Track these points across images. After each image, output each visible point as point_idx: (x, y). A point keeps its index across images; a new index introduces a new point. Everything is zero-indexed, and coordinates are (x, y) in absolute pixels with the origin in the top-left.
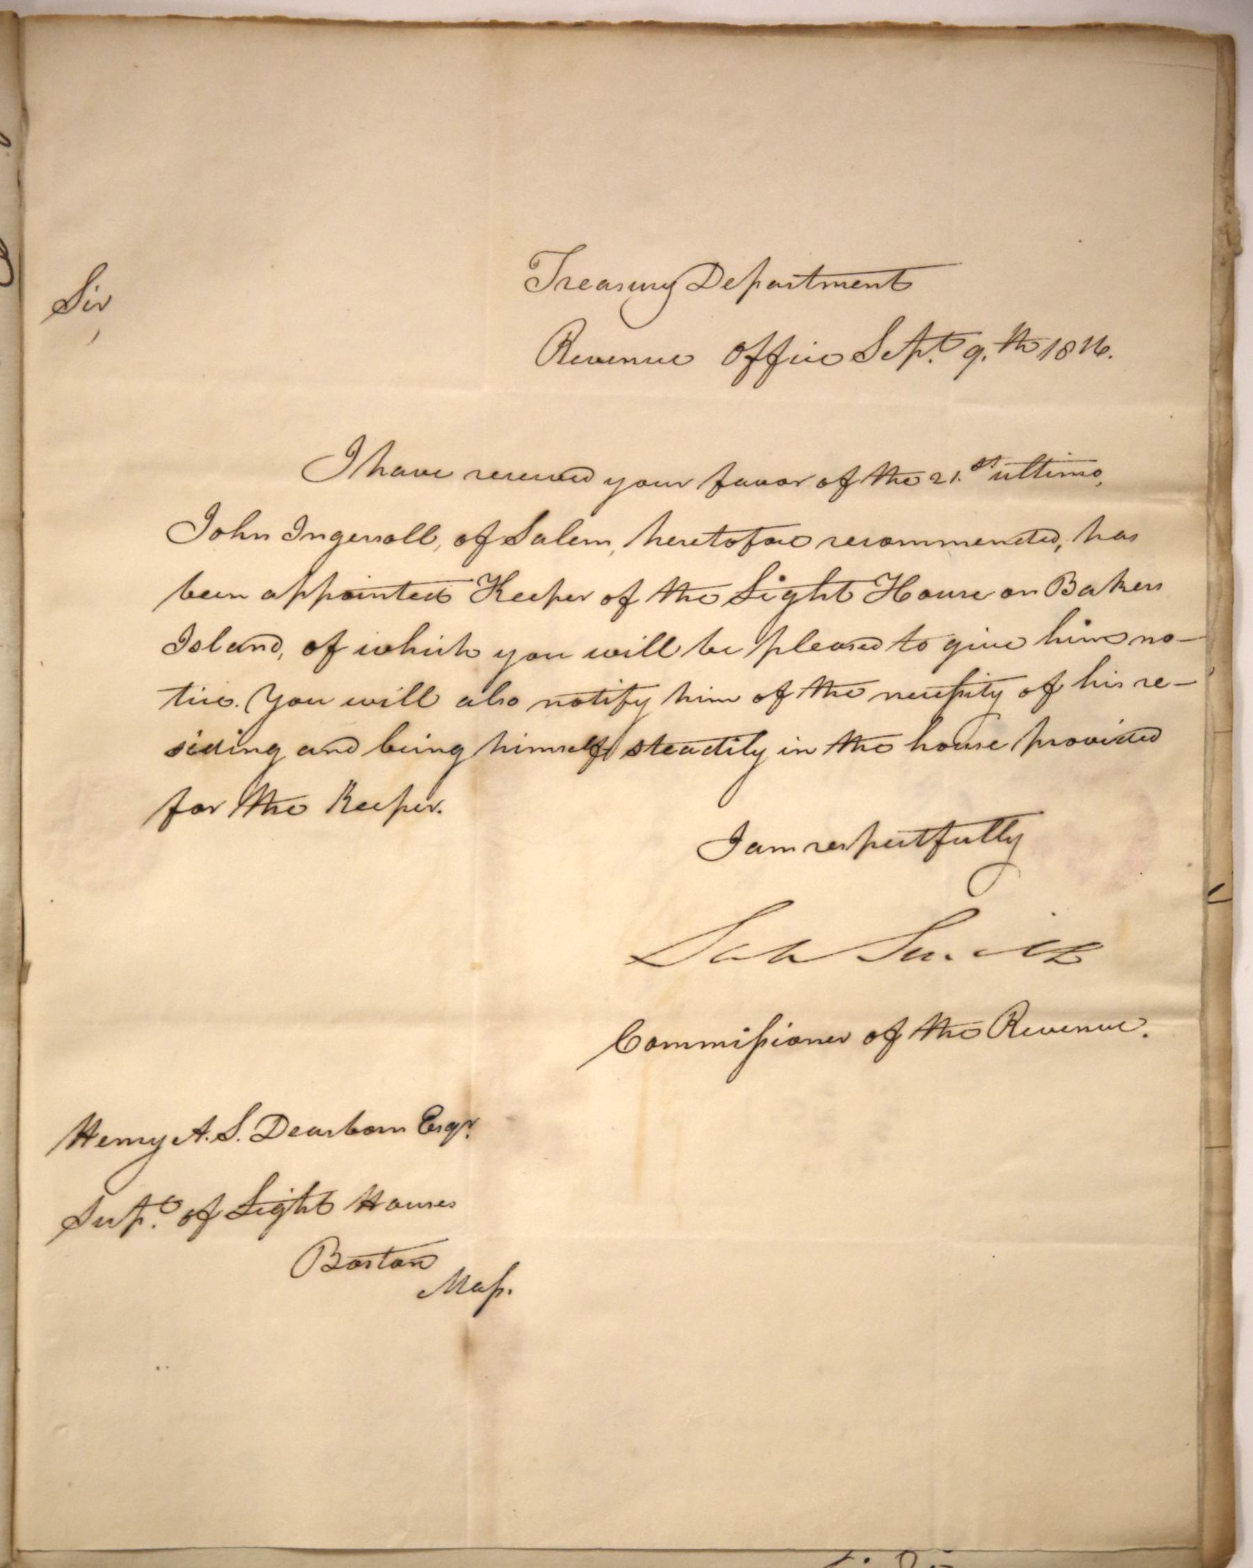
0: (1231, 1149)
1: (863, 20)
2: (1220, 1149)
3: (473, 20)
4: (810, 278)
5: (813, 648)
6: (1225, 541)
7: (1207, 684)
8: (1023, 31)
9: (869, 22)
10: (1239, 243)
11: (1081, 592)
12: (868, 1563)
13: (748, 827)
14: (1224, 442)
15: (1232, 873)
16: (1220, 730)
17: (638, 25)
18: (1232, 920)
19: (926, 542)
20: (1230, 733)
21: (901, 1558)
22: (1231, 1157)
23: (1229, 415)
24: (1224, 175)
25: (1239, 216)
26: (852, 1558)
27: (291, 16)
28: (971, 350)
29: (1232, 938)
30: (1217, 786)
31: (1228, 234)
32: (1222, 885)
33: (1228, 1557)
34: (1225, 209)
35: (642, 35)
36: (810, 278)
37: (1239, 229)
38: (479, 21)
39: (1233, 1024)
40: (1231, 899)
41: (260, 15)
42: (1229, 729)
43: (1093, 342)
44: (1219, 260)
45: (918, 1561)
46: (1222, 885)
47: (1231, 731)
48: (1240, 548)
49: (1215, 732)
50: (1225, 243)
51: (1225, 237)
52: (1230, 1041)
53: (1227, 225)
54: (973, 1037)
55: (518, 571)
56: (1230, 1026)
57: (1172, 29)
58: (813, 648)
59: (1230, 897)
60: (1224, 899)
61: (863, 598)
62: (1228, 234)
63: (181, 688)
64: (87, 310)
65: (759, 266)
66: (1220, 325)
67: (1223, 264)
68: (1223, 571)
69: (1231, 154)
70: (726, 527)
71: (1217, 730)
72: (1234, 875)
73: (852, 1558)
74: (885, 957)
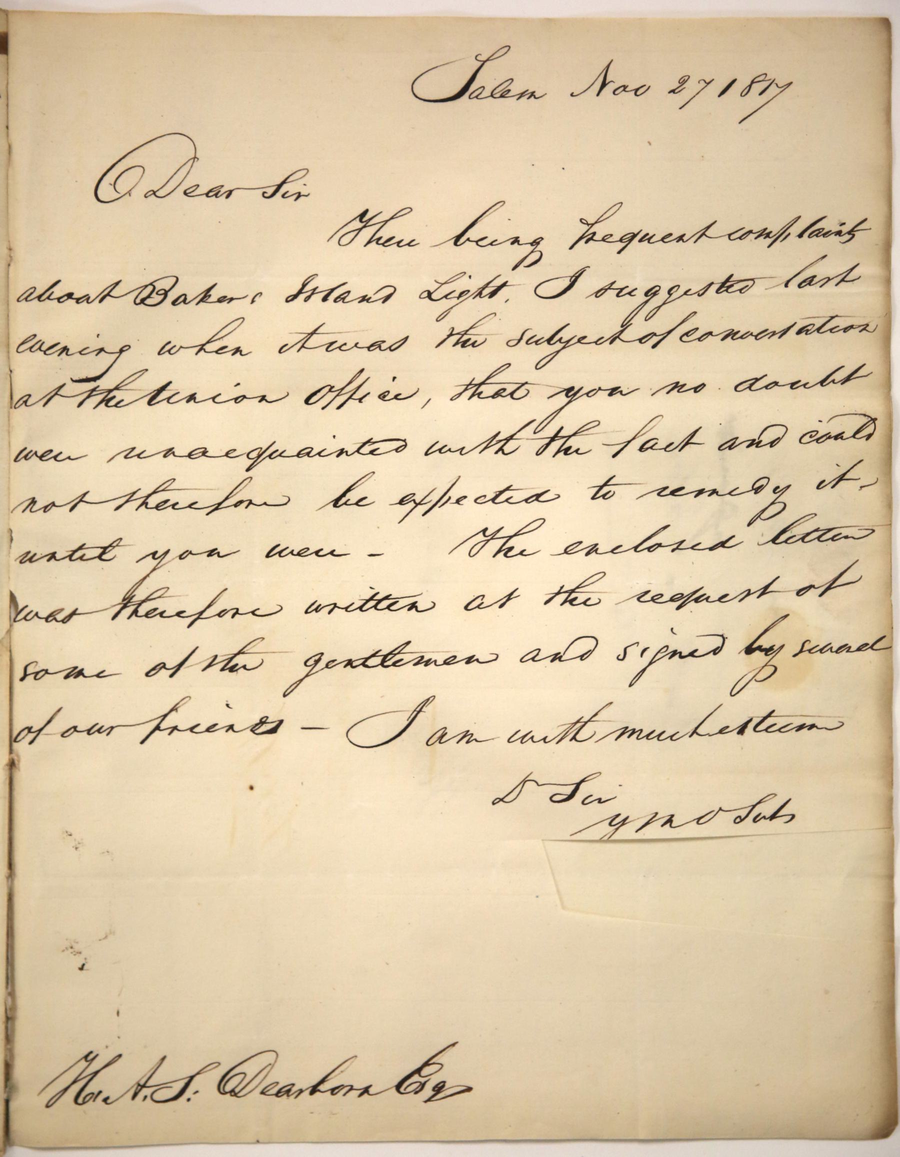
4: (477, 387)
5: (372, 452)
11: (17, 457)
13: (650, 660)
15: (892, 628)
18: (892, 662)
20: (889, 526)
22: (893, 836)
28: (10, 613)
32: (884, 637)
36: (477, 387)
39: (894, 739)
42: (889, 523)
46: (884, 637)
47: (891, 525)
58: (372, 452)
59: (890, 646)
60: (885, 647)
61: (770, 480)
63: (365, 600)
64: (523, 662)
72: (894, 630)
74: (166, 277)
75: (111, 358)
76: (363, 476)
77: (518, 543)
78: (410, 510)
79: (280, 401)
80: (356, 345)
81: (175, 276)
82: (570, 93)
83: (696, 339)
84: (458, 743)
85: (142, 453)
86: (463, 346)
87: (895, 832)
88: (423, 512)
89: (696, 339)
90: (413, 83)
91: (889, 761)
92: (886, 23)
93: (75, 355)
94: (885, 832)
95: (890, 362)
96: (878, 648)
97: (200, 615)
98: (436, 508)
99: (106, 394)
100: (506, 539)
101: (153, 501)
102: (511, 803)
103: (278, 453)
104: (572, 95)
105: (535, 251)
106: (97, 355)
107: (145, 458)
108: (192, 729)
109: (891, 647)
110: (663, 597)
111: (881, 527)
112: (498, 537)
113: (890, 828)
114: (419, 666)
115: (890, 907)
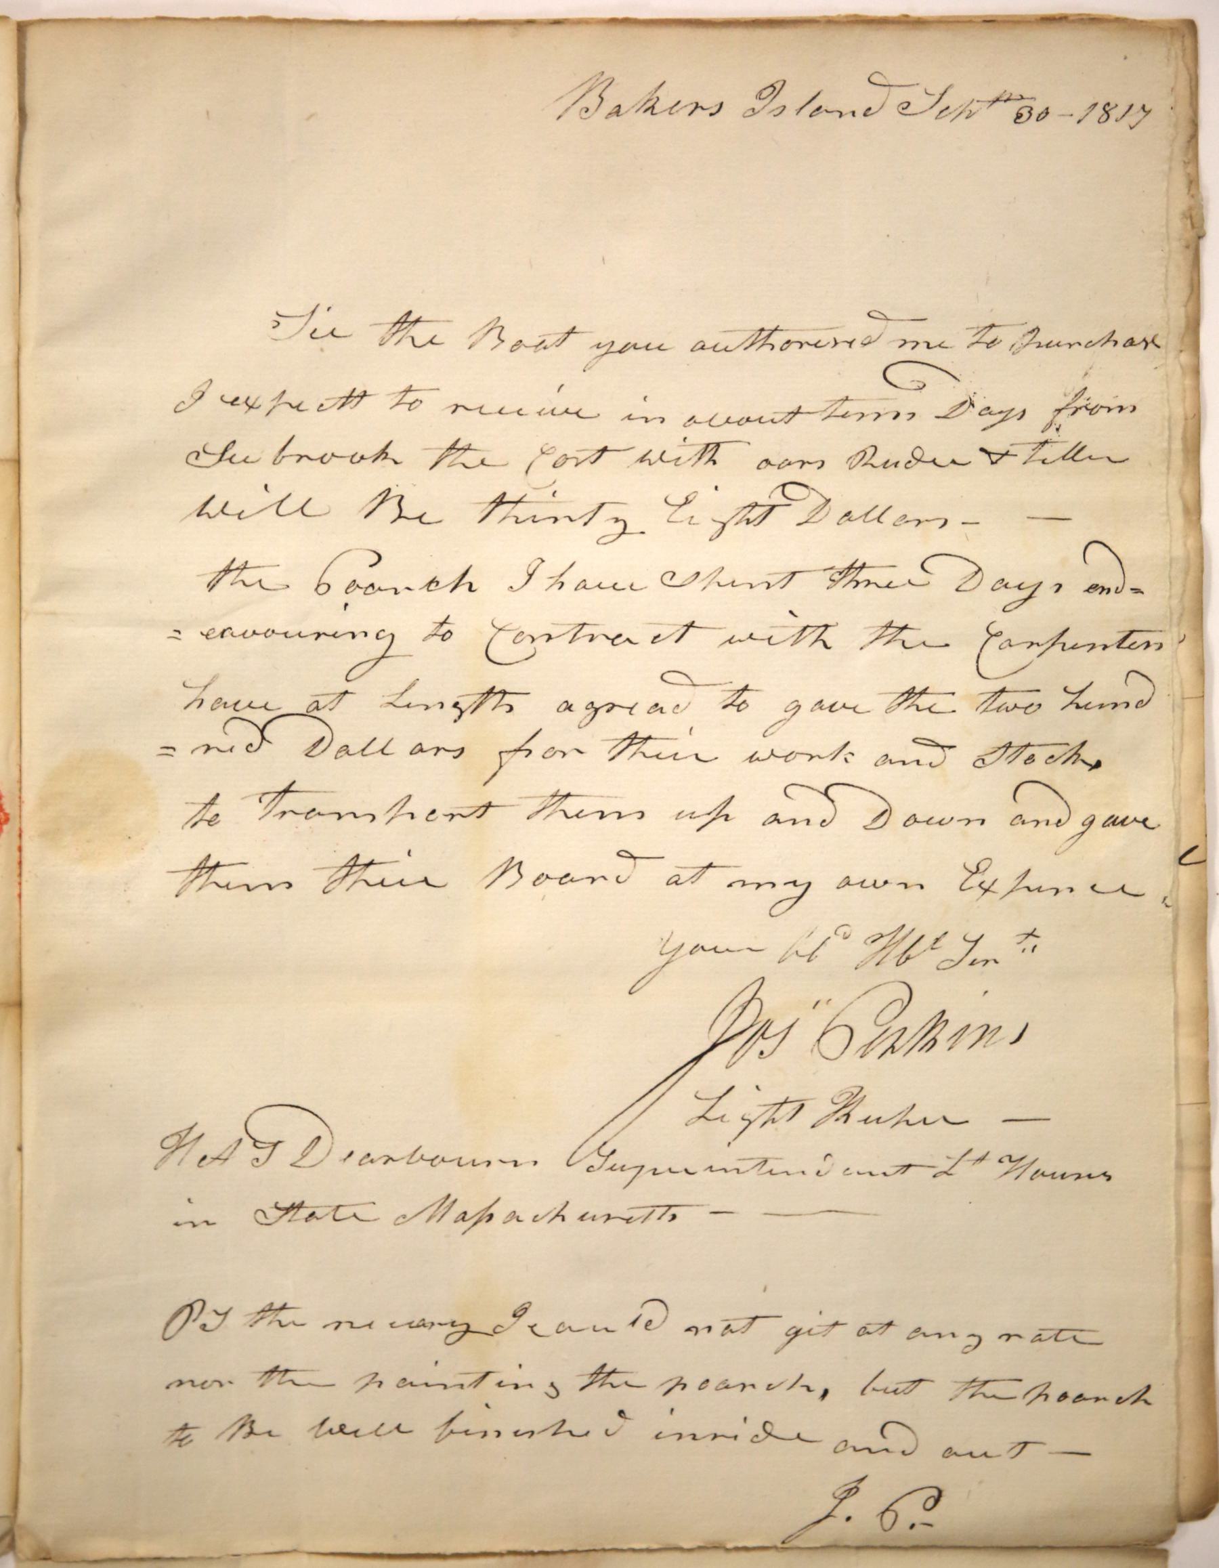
0: (1209, 1105)
1: (832, 13)
2: (1199, 1106)
3: (452, 18)
6: (1193, 511)
7: (1175, 652)
8: (989, 21)
9: (839, 16)
10: (1202, 227)
12: (849, 1522)
14: (1190, 415)
16: (1190, 696)
17: (614, 21)
19: (738, 1172)
21: (882, 1517)
22: (1209, 1114)
23: (1197, 388)
24: (1187, 161)
25: (1202, 200)
26: (834, 1517)
27: (277, 15)
29: (1207, 900)
30: (1189, 751)
31: (1191, 217)
32: (1196, 847)
33: (1211, 1506)
34: (1188, 193)
35: (618, 30)
37: (1202, 214)
38: (459, 19)
40: (1205, 861)
41: (246, 15)
42: (1201, 695)
43: (886, 639)
44: (1183, 243)
45: (899, 1519)
46: (1196, 847)
47: (1203, 696)
48: (1207, 519)
49: (1183, 699)
50: (1189, 226)
51: (1189, 221)
52: (1206, 1000)
53: (1190, 208)
54: (888, 818)
55: (914, 741)
56: (1206, 985)
57: (1135, 21)
62: (1191, 217)
65: (930, 1021)
66: (1185, 306)
67: (1187, 247)
68: (1191, 542)
69: (1193, 141)
70: (574, 328)
71: (1185, 697)
73: (834, 1517)
79: (711, 1023)
80: (398, 1428)
82: (291, 889)
83: (755, 1120)
87: (1211, 1109)
89: (755, 1120)
91: (1204, 1012)
92: (1191, 26)
93: (1085, 461)
94: (1199, 1109)
95: (1199, 478)
96: (1188, 862)
102: (1100, 540)
104: (290, 885)
108: (927, 822)
109: (1205, 861)
111: (1192, 700)
113: (1205, 1103)
115: (1206, 1209)
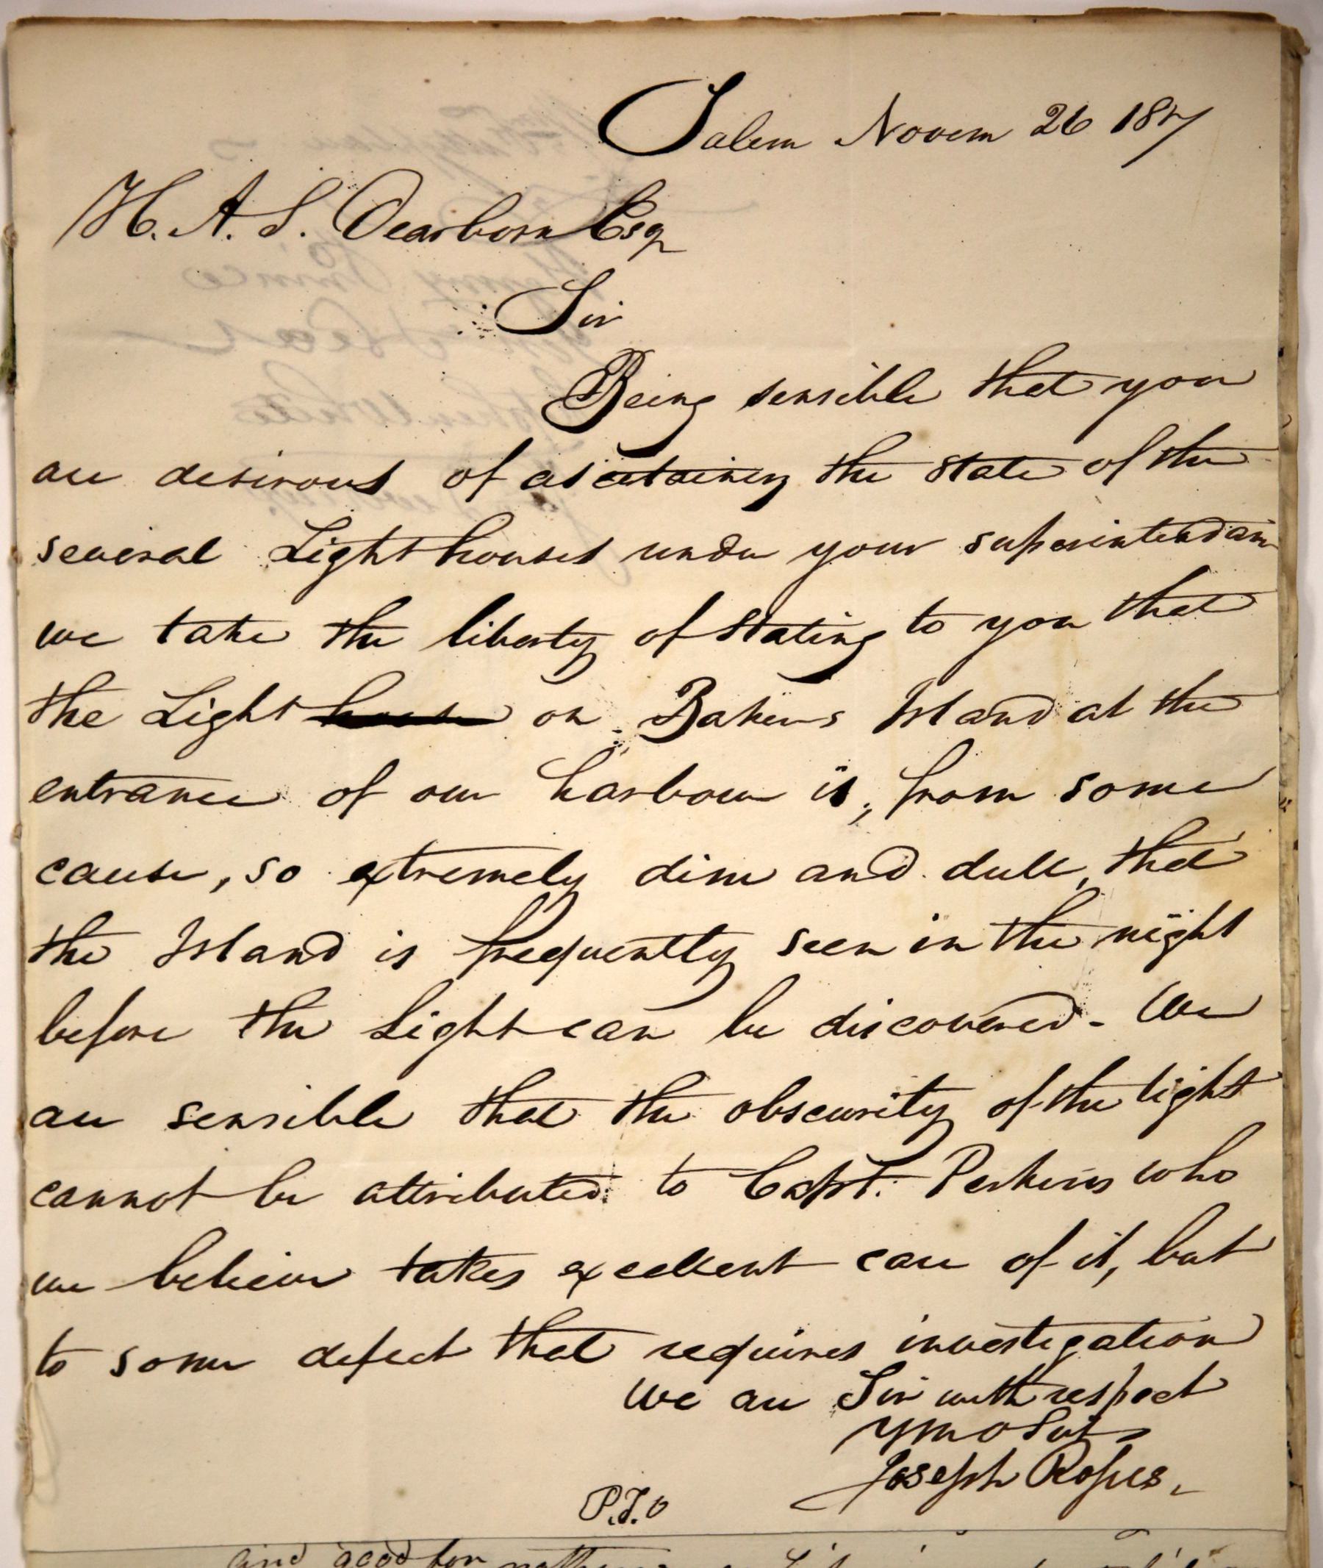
22: (1305, 1439)
75: (574, 393)
76: (1234, 612)
77: (84, 705)
78: (195, 935)
81: (987, 1145)
84: (839, 543)
85: (161, 1031)
86: (652, 1120)
88: (1010, 363)
90: (608, 1354)
97: (364, 1360)
98: (1111, 1407)
99: (66, 703)
100: (1061, 376)
101: (581, 786)
103: (64, 635)
105: (803, 625)
106: (981, 453)
107: (165, 1040)
110: (103, 716)
112: (421, 548)
114: (974, 141)
